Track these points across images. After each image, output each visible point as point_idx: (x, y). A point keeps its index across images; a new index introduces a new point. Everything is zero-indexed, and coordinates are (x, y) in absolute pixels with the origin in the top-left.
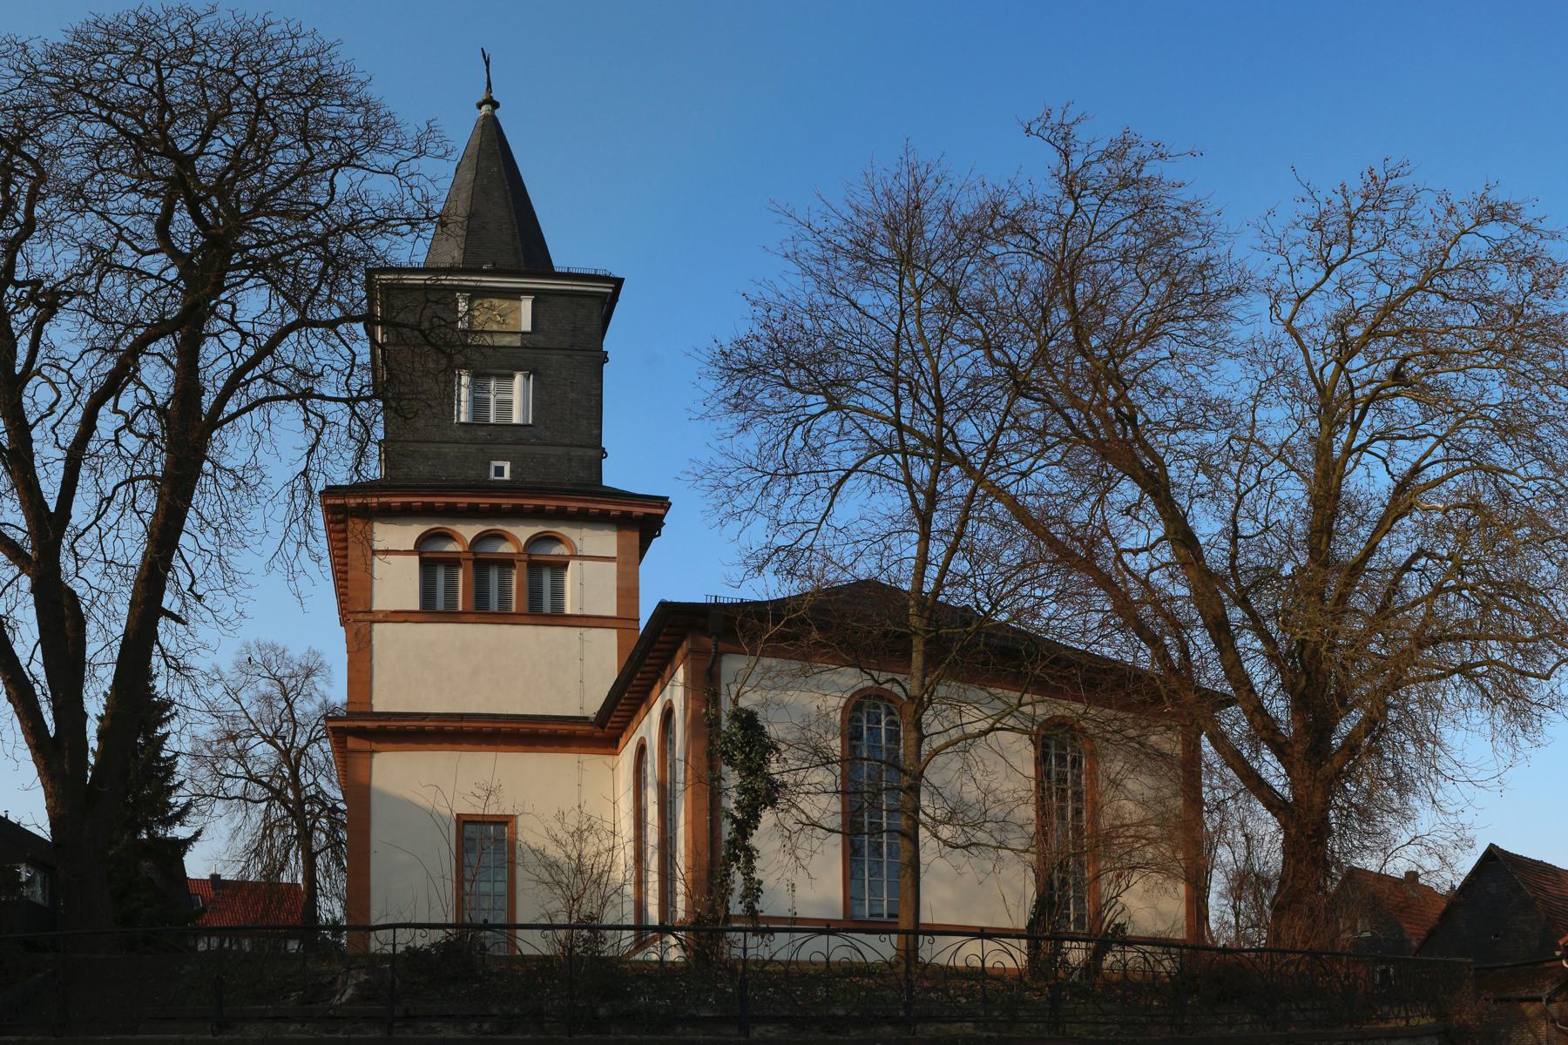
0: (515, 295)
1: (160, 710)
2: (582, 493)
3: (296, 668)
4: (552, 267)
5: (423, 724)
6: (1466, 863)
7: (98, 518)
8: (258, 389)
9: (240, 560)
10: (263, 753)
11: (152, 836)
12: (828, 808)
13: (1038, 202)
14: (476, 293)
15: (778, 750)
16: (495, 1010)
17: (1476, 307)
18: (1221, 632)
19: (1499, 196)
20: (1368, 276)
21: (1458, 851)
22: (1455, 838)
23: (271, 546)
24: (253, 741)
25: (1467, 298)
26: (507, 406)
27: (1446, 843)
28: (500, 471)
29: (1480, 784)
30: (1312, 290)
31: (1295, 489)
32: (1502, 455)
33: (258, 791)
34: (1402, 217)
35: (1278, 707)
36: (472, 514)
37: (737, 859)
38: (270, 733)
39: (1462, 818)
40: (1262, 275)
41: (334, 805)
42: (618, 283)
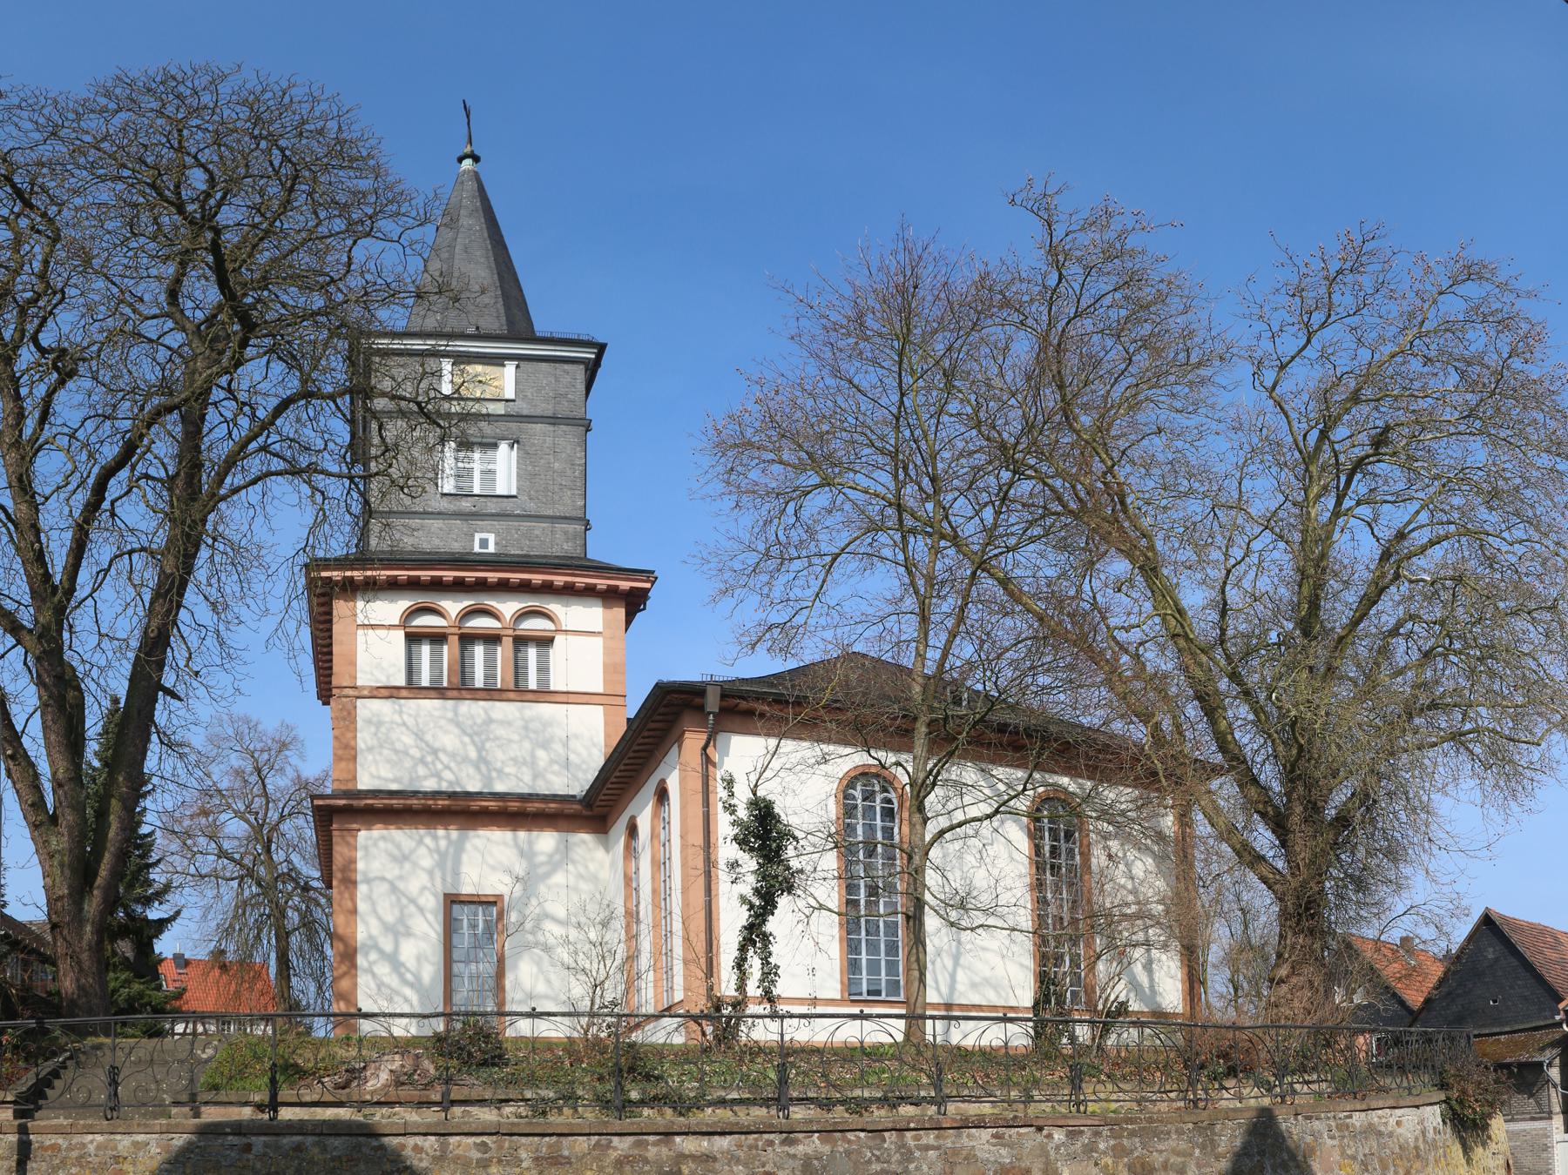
0: (498, 360)
1: (138, 786)
2: (569, 567)
3: (269, 742)
4: (533, 331)
5: (409, 802)
6: (1461, 932)
7: (94, 591)
8: (255, 465)
9: (238, 637)
10: (235, 828)
11: (130, 915)
12: (830, 894)
13: (1024, 275)
14: (461, 359)
15: (795, 838)
16: (528, 1095)
17: (1456, 369)
18: (1211, 709)
19: (1475, 254)
20: (1349, 342)
21: (1454, 919)
22: (1452, 907)
23: (269, 624)
24: (223, 817)
25: (1447, 358)
26: (490, 476)
27: (1442, 912)
28: (484, 543)
29: (1472, 854)
30: (1293, 358)
31: (1281, 558)
32: (1487, 517)
33: (231, 869)
34: (1380, 281)
35: (1269, 775)
36: (459, 587)
37: (754, 943)
38: (242, 808)
39: (1457, 887)
40: (1244, 343)
41: (306, 883)
42: (601, 348)
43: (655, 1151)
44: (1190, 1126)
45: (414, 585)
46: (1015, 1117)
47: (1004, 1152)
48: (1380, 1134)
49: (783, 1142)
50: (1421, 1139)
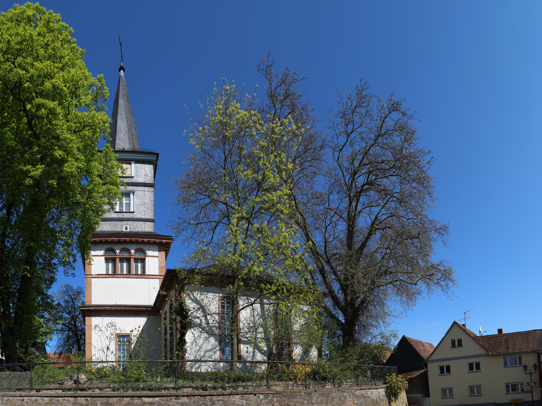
28: (126, 228)
43: (136, 401)
44: (303, 394)
45: (107, 242)
46: (248, 391)
47: (244, 401)
48: (365, 397)
49: (175, 399)
50: (378, 399)
